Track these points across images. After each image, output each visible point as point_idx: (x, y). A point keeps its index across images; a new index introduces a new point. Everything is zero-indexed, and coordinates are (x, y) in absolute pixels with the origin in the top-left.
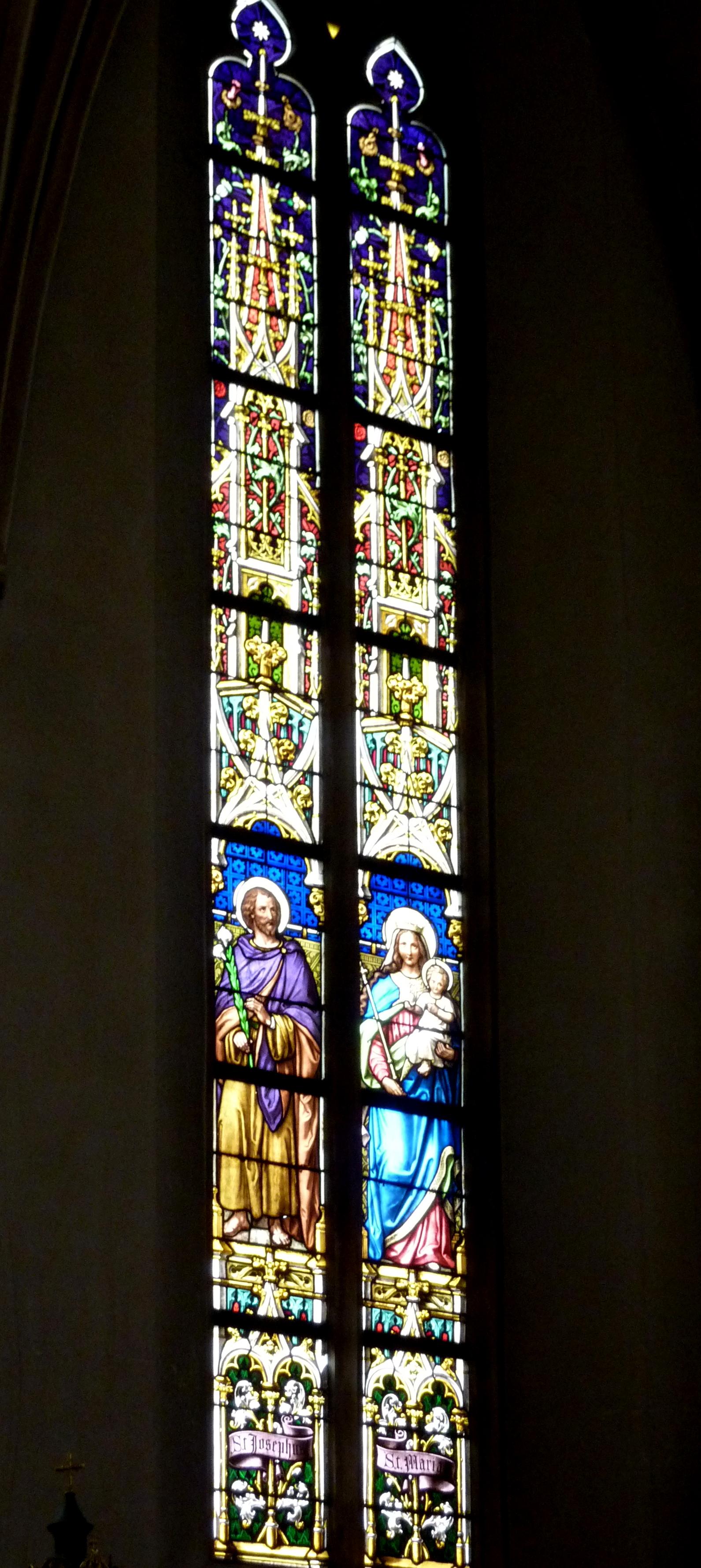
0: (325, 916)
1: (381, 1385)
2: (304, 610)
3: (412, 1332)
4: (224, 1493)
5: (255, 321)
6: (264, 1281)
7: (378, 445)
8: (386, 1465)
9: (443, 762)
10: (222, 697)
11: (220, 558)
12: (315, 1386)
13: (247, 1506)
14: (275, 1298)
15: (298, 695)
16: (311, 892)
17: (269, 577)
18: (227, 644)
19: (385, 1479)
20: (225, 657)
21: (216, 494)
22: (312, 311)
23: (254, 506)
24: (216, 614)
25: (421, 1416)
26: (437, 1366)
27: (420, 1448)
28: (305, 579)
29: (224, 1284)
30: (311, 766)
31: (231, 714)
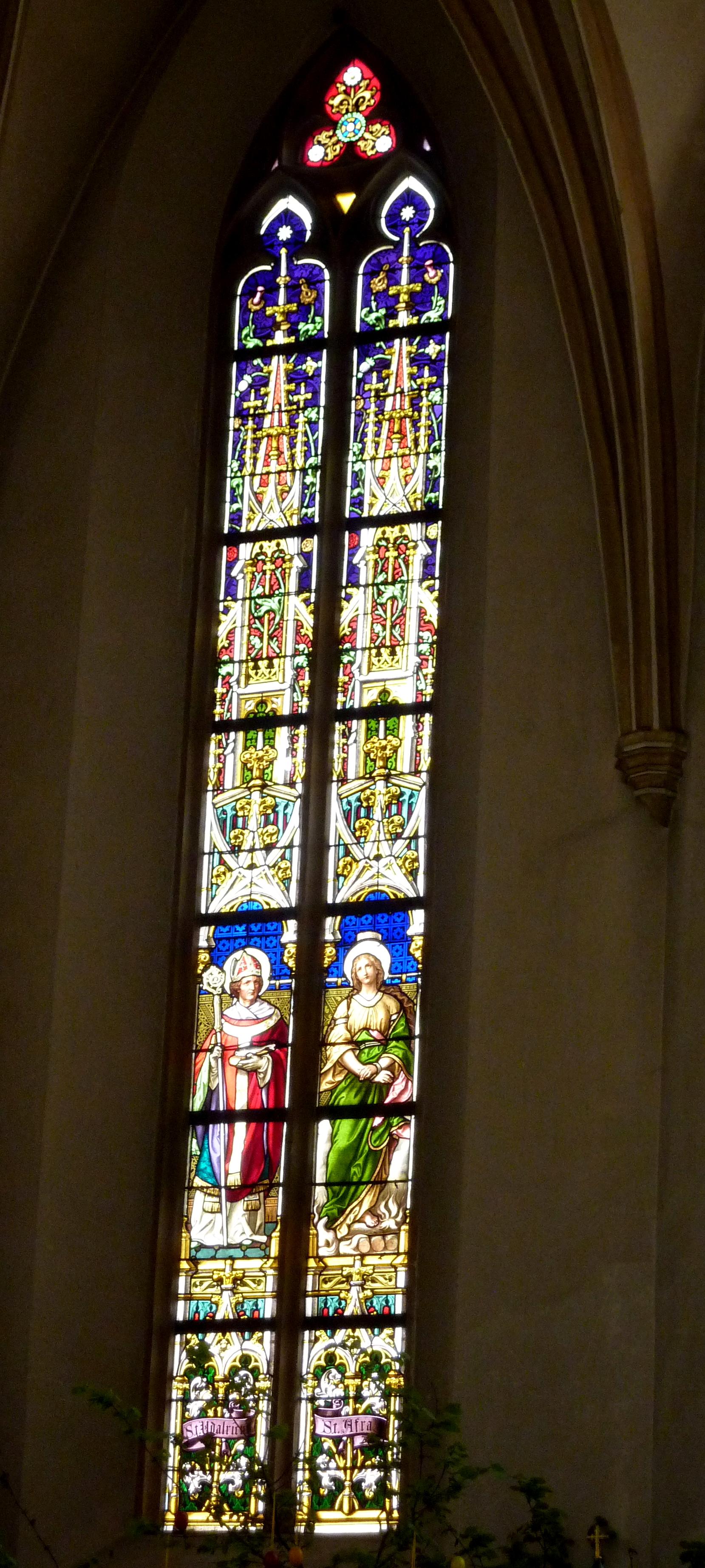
0: (296, 967)
1: (322, 1363)
2: (419, 700)
3: (226, 1315)
4: (176, 1473)
5: (387, 468)
6: (222, 1290)
7: (248, 558)
8: (324, 1431)
9: (288, 811)
10: (217, 809)
11: (345, 683)
12: (261, 1372)
13: (194, 1482)
14: (231, 1303)
15: (285, 784)
16: (286, 948)
17: (387, 683)
18: (224, 764)
19: (322, 1443)
20: (221, 777)
21: (345, 629)
22: (440, 439)
23: (378, 628)
24: (339, 730)
25: (359, 1383)
26: (376, 1338)
27: (355, 1412)
28: (420, 673)
29: (316, 1294)
30: (417, 832)
31: (225, 821)
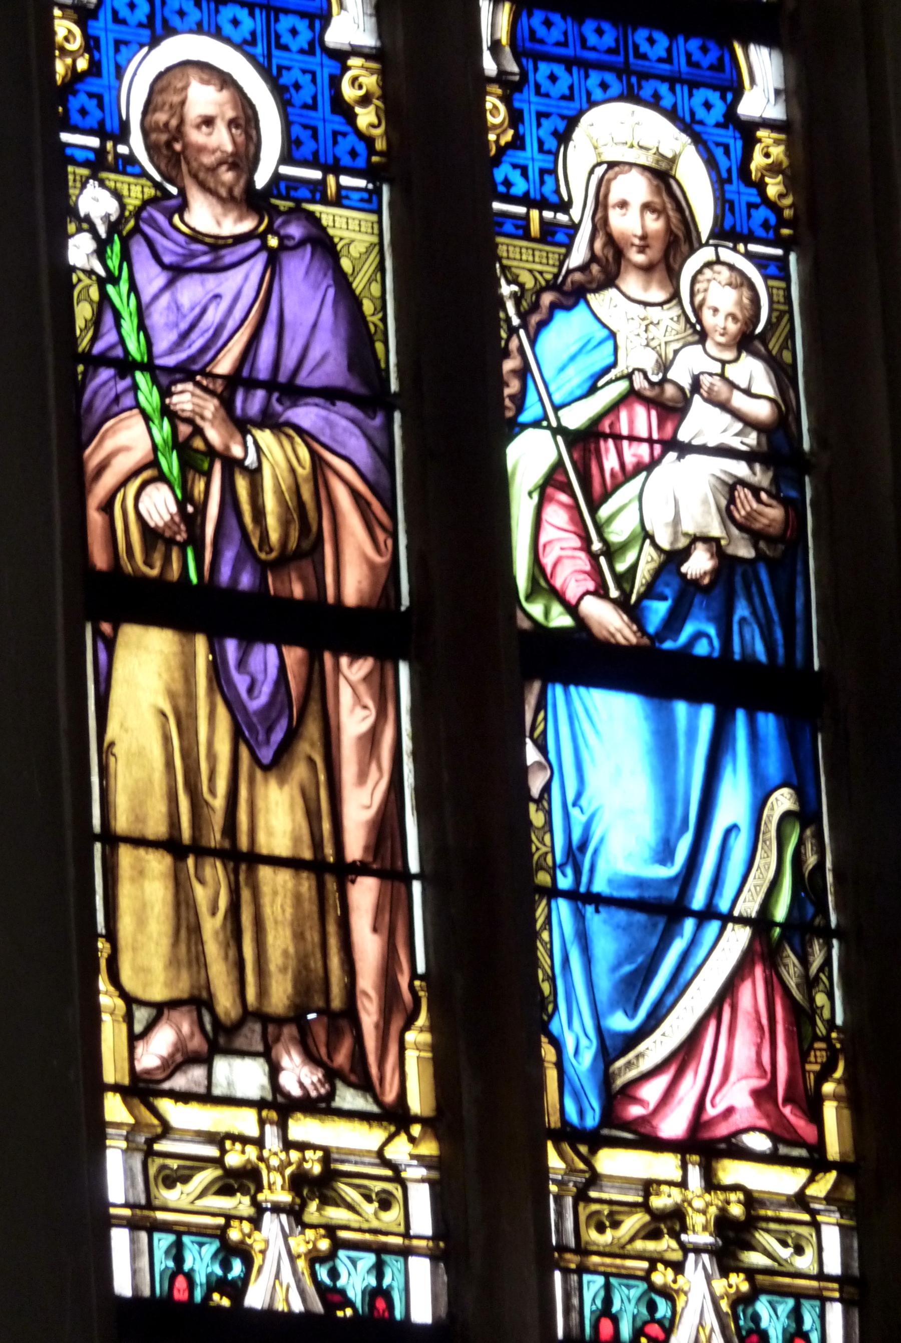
6: (260, 1209)
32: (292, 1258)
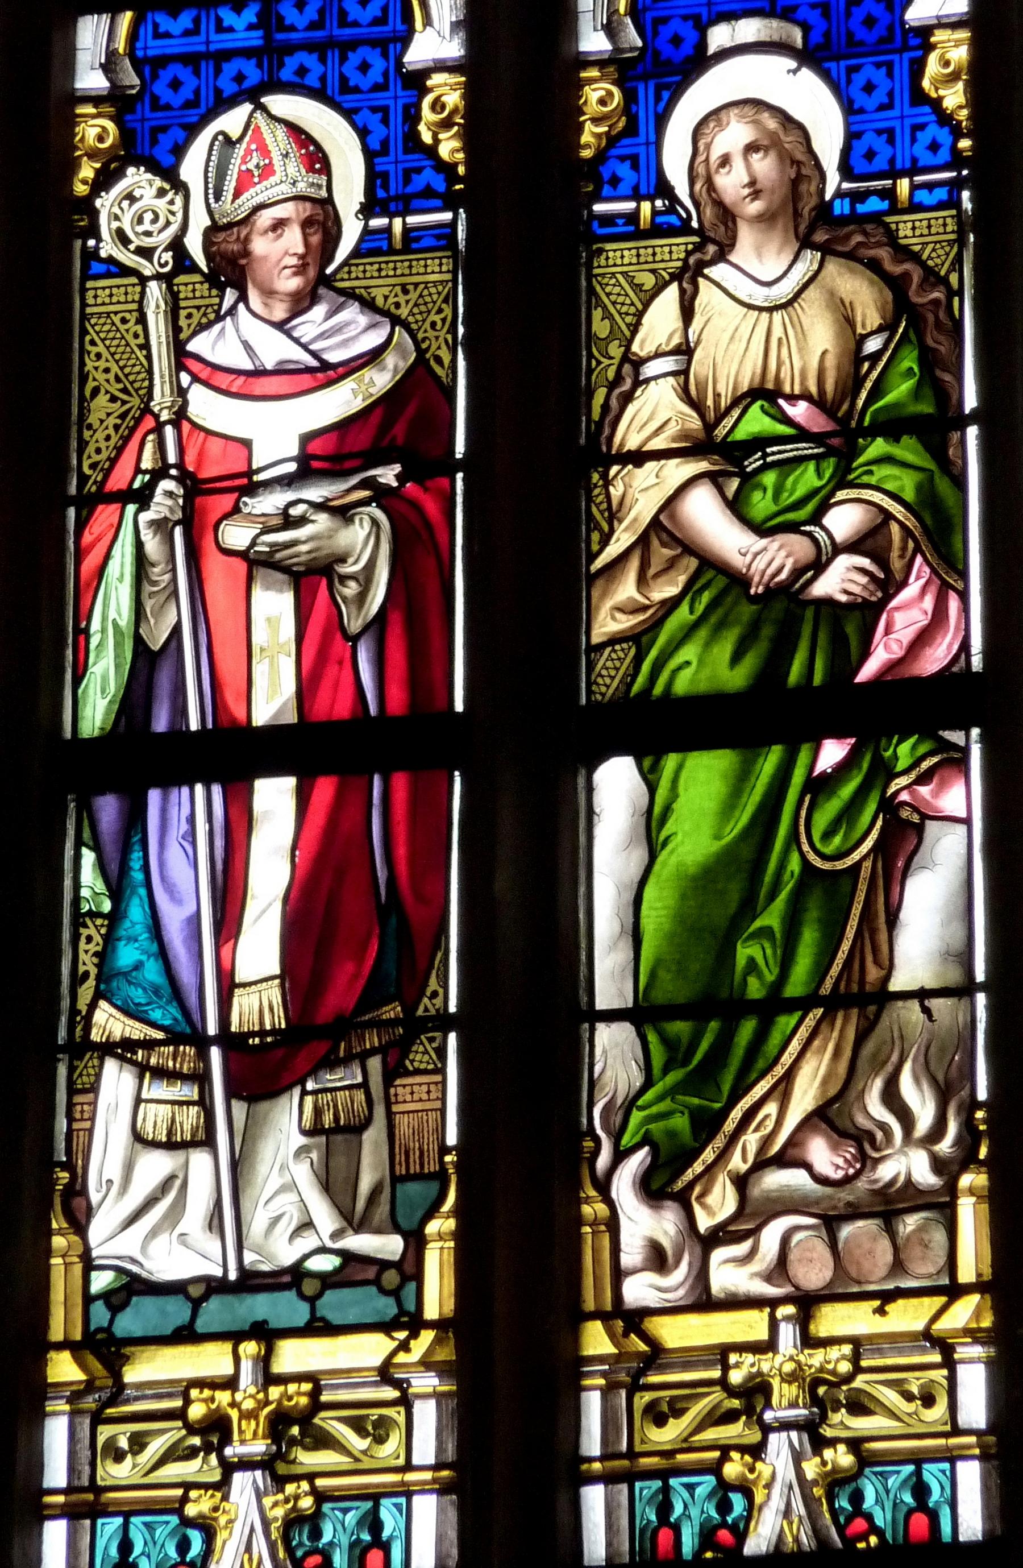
32: (266, 1523)
